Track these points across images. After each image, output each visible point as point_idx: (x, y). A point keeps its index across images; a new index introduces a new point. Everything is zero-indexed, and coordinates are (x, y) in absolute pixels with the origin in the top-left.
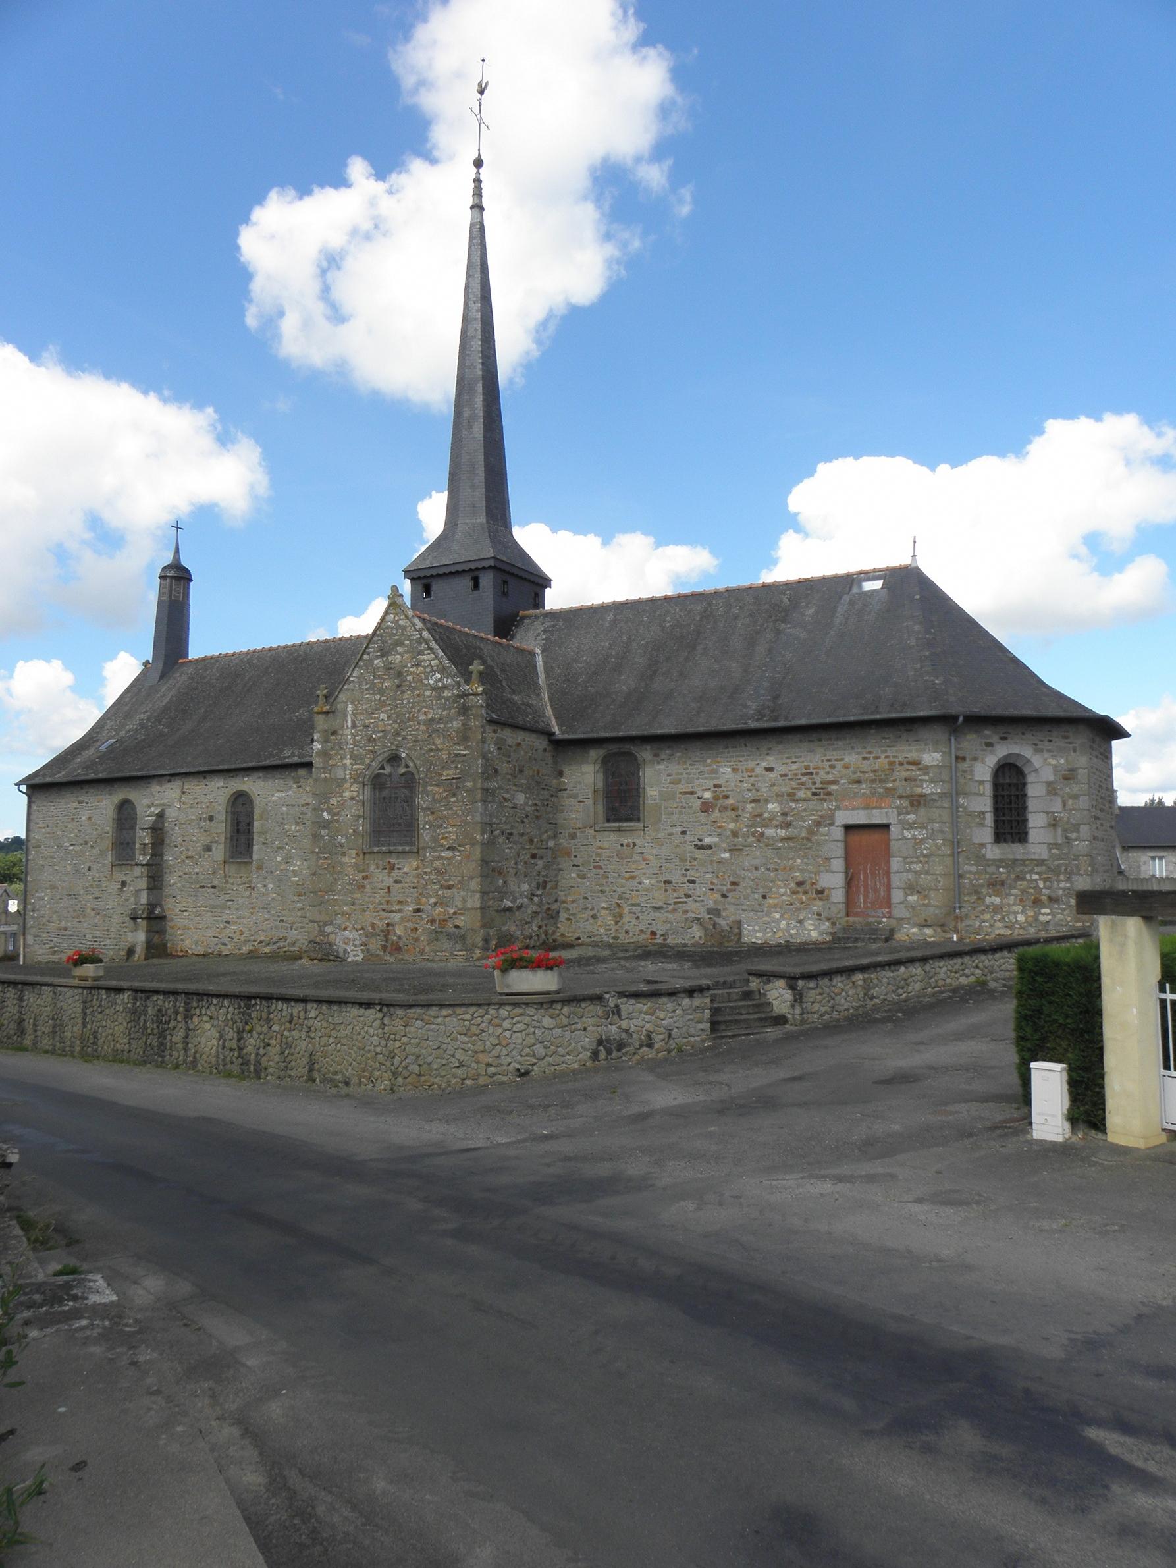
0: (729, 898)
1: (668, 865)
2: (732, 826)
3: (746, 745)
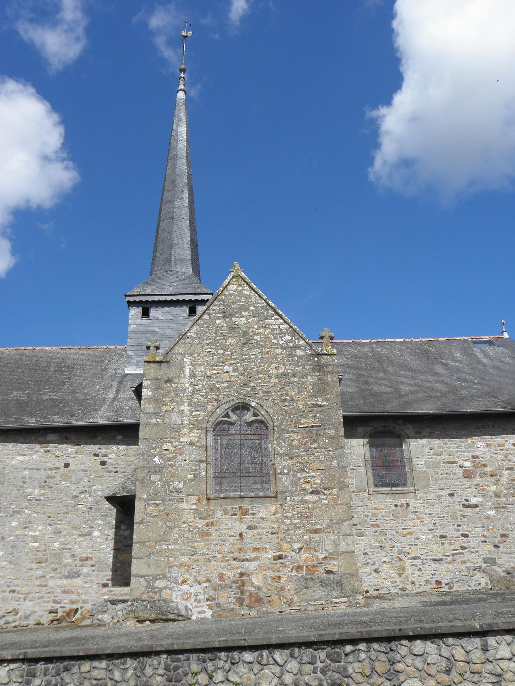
0: (502, 547)
1: (441, 522)
2: (493, 488)
3: (494, 427)
